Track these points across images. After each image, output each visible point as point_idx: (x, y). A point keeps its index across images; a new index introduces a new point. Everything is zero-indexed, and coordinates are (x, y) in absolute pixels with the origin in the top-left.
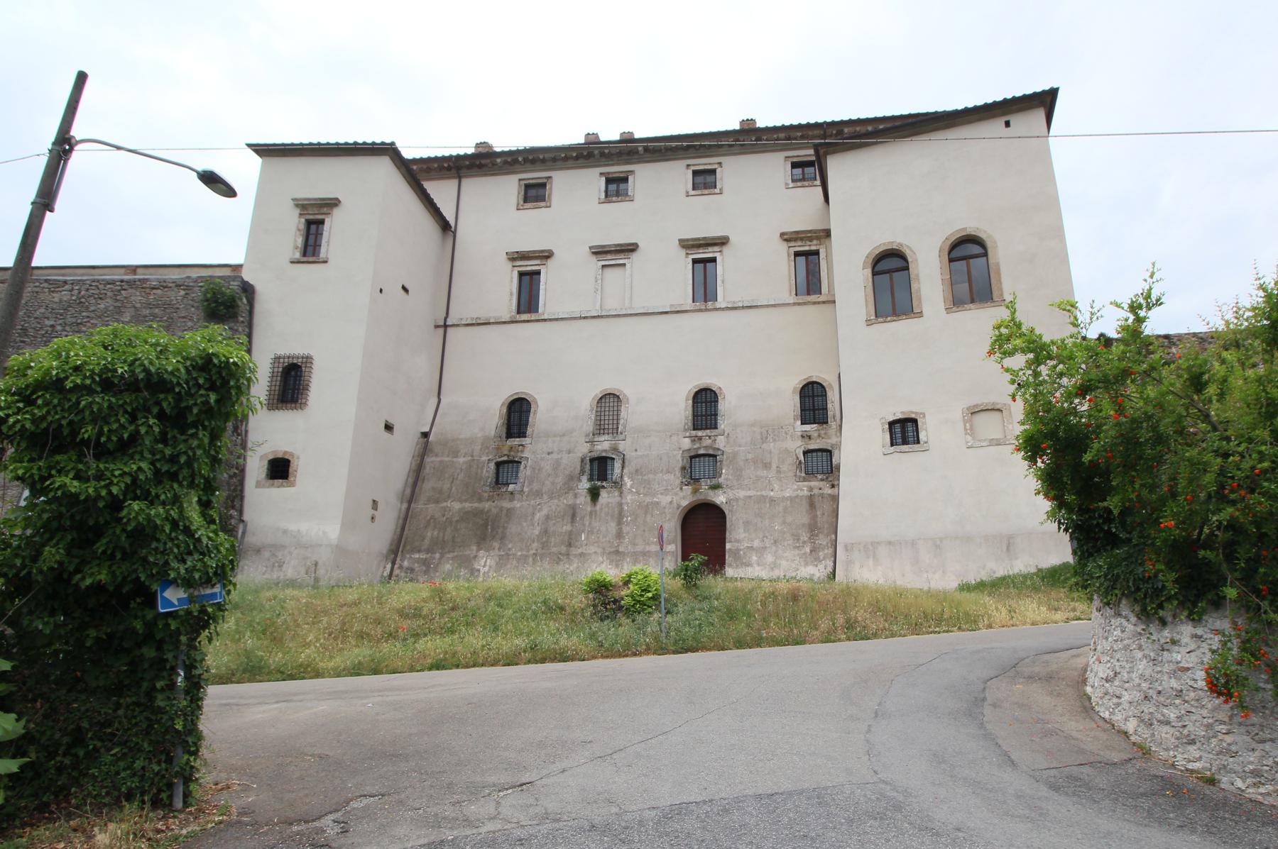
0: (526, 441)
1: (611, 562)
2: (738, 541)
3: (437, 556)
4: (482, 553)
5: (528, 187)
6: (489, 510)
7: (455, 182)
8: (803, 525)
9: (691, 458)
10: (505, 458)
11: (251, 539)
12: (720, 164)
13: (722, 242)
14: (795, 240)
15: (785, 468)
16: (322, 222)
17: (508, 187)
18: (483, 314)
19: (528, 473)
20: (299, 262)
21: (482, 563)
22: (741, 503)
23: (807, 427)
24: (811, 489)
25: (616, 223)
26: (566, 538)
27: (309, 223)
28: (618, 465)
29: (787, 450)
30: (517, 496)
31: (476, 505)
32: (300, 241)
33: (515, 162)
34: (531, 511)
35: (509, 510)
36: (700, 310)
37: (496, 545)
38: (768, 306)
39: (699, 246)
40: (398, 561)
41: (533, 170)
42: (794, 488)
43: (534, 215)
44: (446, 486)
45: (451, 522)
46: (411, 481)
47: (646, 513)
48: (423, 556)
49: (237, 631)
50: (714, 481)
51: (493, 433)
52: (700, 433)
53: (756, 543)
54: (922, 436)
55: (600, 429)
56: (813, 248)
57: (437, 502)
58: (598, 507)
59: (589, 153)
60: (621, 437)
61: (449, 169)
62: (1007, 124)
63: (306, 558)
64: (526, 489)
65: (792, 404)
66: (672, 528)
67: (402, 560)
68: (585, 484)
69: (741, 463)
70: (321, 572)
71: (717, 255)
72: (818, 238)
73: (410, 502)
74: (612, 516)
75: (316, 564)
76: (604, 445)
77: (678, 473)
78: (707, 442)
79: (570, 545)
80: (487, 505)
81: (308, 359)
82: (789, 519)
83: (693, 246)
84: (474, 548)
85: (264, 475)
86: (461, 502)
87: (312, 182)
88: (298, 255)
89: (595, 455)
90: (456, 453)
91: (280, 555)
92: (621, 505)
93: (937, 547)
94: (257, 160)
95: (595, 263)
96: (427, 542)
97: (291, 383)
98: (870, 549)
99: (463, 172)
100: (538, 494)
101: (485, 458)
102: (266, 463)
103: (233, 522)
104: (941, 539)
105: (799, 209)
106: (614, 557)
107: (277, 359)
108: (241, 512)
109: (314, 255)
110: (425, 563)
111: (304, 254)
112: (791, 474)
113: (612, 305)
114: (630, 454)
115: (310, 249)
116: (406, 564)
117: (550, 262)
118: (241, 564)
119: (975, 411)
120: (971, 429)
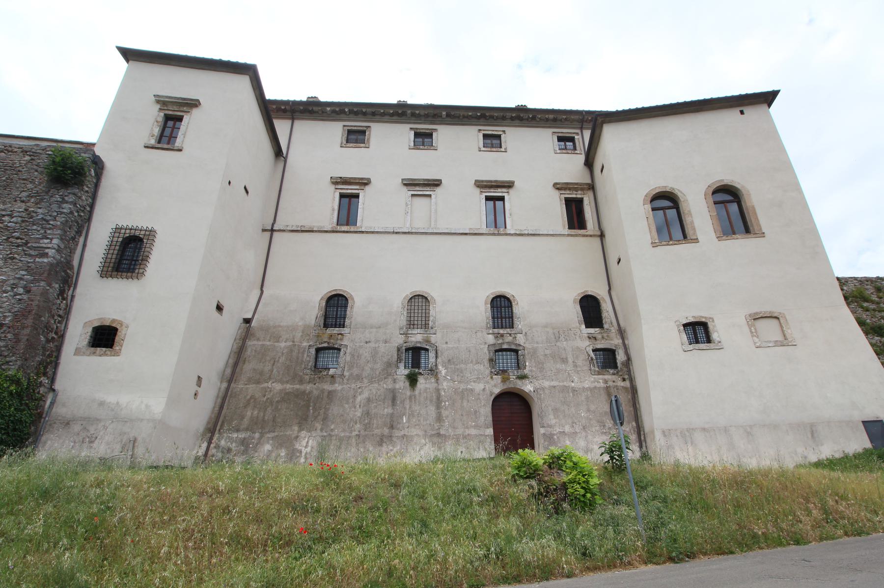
0: (345, 331)
1: (434, 444)
2: (550, 426)
3: (257, 435)
4: (303, 433)
5: (350, 132)
6: (310, 393)
7: (290, 122)
8: (606, 413)
9: (496, 351)
10: (325, 345)
11: (60, 410)
12: (504, 131)
13: (509, 185)
14: (565, 189)
15: (580, 362)
16: (180, 119)
17: (335, 130)
18: (307, 223)
19: (348, 358)
20: (153, 148)
21: (304, 443)
22: (547, 392)
23: (592, 330)
24: (606, 382)
25: (423, 164)
26: (388, 420)
27: (167, 118)
28: (432, 355)
29: (578, 348)
30: (338, 380)
31: (298, 386)
32: (157, 131)
33: (342, 112)
34: (357, 391)
35: (330, 392)
36: (494, 234)
37: (318, 426)
38: (547, 235)
39: (491, 187)
40: (215, 439)
41: (358, 119)
42: (593, 381)
43: (354, 153)
44: (267, 368)
45: (271, 403)
46: (231, 361)
47: (462, 398)
48: (242, 435)
49: (46, 536)
50: (520, 372)
51: (313, 322)
52: (501, 331)
53: (567, 429)
54: (715, 336)
55: (411, 324)
56: (579, 196)
57: (258, 382)
58: (417, 392)
59: (400, 112)
60: (432, 331)
61: (285, 111)
62: (742, 112)
63: (122, 434)
64: (346, 374)
65: (575, 313)
66: (486, 412)
67: (219, 440)
68: (403, 371)
69: (542, 357)
70: (140, 451)
71: (505, 195)
72: (582, 189)
73: (230, 382)
74: (431, 401)
75: (135, 441)
76: (417, 337)
77: (487, 364)
78: (509, 339)
79: (392, 427)
80: (308, 387)
81: (151, 233)
82: (593, 407)
83: (486, 187)
84: (296, 428)
85: (86, 342)
86: (282, 382)
87: (174, 89)
88: (153, 142)
89: (411, 345)
90: (278, 339)
91: (92, 430)
92: (438, 390)
93: (749, 434)
94: (122, 64)
95: (406, 193)
96: (246, 422)
97: (129, 254)
98: (687, 435)
99: (297, 114)
100: (359, 378)
101: (305, 344)
102: (90, 330)
103: (42, 390)
104: (751, 427)
105: (571, 167)
106: (435, 439)
107: (118, 230)
108: (53, 380)
109: (168, 143)
110: (243, 442)
111: (159, 142)
112: (586, 368)
113: (420, 225)
114: (441, 346)
115: (165, 139)
116: (223, 443)
117: (367, 188)
118: (44, 438)
119: (757, 318)
120: (756, 332)
